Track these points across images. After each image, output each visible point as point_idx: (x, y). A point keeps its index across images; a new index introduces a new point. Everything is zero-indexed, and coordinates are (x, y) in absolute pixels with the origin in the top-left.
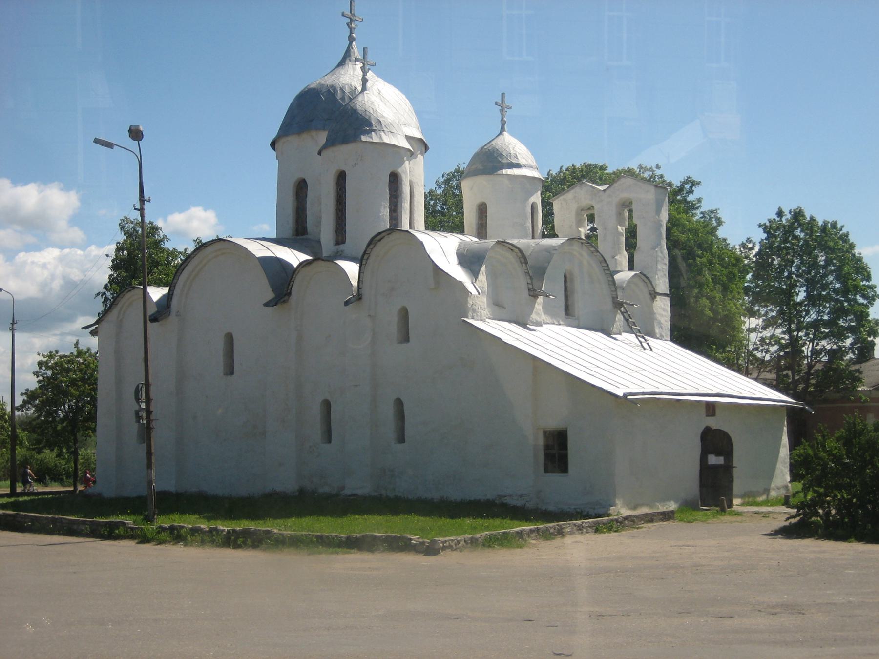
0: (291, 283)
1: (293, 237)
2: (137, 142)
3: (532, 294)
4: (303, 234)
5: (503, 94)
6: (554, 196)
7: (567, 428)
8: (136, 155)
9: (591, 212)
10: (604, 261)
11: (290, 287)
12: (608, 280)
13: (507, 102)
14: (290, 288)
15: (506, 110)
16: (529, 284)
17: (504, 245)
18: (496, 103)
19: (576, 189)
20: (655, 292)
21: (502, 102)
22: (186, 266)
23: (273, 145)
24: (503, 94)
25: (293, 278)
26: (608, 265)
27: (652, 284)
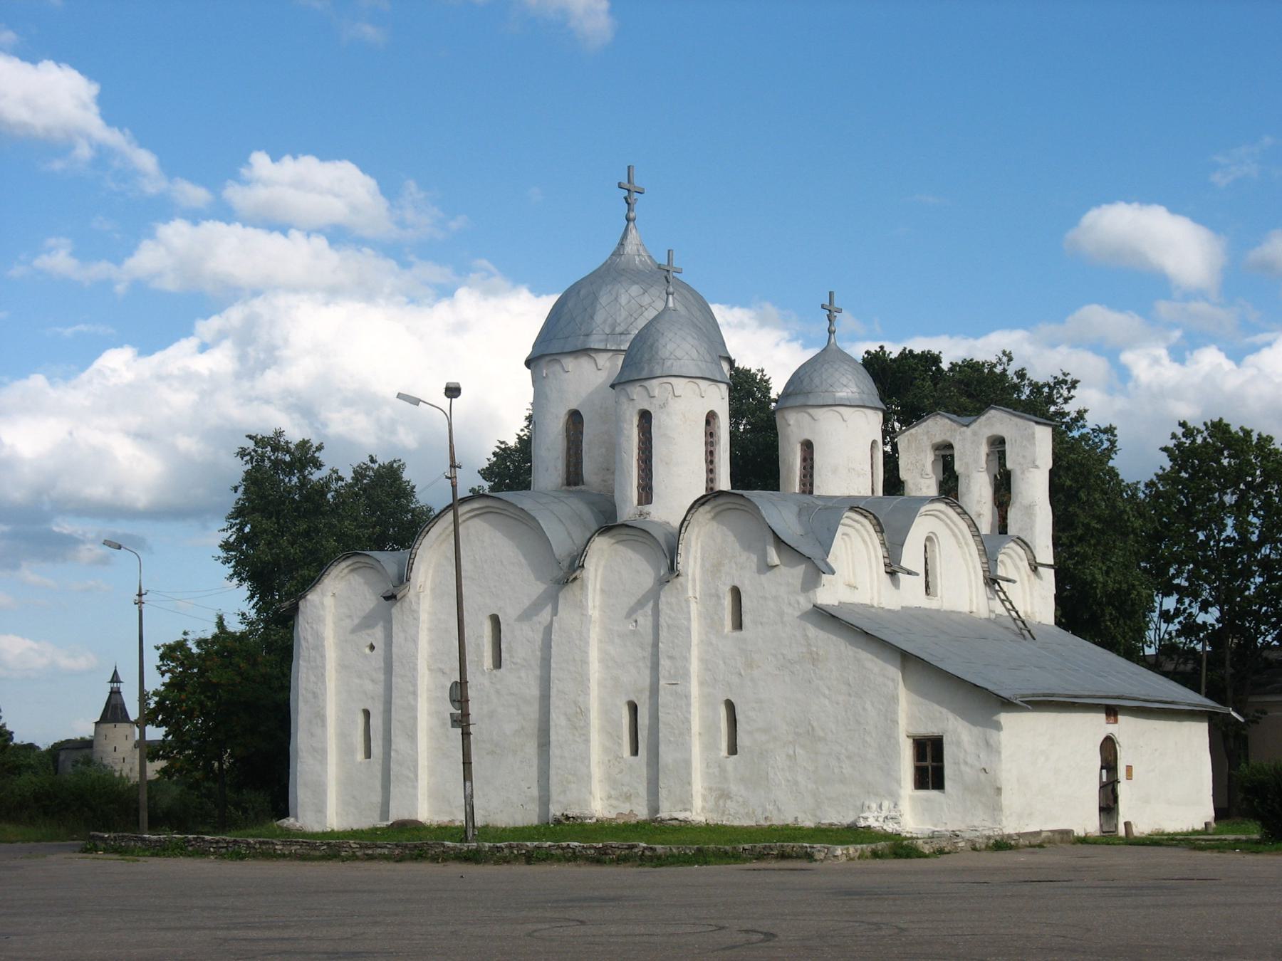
0: (585, 553)
1: (564, 488)
2: (449, 399)
3: (889, 570)
4: (576, 484)
5: (831, 294)
6: (1230, 777)
7: (942, 736)
8: (444, 412)
9: (948, 453)
10: (973, 525)
11: (583, 558)
12: (978, 549)
13: (837, 304)
14: (582, 560)
15: (835, 314)
16: (886, 557)
17: (856, 511)
18: (823, 307)
19: (928, 421)
20: (1036, 562)
21: (830, 304)
22: (433, 526)
23: (528, 363)
24: (831, 294)
25: (587, 548)
26: (978, 530)
27: (1032, 552)
